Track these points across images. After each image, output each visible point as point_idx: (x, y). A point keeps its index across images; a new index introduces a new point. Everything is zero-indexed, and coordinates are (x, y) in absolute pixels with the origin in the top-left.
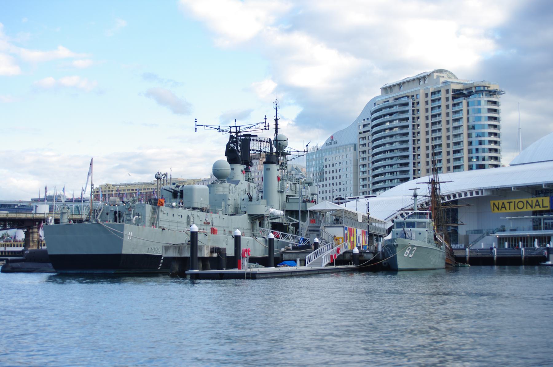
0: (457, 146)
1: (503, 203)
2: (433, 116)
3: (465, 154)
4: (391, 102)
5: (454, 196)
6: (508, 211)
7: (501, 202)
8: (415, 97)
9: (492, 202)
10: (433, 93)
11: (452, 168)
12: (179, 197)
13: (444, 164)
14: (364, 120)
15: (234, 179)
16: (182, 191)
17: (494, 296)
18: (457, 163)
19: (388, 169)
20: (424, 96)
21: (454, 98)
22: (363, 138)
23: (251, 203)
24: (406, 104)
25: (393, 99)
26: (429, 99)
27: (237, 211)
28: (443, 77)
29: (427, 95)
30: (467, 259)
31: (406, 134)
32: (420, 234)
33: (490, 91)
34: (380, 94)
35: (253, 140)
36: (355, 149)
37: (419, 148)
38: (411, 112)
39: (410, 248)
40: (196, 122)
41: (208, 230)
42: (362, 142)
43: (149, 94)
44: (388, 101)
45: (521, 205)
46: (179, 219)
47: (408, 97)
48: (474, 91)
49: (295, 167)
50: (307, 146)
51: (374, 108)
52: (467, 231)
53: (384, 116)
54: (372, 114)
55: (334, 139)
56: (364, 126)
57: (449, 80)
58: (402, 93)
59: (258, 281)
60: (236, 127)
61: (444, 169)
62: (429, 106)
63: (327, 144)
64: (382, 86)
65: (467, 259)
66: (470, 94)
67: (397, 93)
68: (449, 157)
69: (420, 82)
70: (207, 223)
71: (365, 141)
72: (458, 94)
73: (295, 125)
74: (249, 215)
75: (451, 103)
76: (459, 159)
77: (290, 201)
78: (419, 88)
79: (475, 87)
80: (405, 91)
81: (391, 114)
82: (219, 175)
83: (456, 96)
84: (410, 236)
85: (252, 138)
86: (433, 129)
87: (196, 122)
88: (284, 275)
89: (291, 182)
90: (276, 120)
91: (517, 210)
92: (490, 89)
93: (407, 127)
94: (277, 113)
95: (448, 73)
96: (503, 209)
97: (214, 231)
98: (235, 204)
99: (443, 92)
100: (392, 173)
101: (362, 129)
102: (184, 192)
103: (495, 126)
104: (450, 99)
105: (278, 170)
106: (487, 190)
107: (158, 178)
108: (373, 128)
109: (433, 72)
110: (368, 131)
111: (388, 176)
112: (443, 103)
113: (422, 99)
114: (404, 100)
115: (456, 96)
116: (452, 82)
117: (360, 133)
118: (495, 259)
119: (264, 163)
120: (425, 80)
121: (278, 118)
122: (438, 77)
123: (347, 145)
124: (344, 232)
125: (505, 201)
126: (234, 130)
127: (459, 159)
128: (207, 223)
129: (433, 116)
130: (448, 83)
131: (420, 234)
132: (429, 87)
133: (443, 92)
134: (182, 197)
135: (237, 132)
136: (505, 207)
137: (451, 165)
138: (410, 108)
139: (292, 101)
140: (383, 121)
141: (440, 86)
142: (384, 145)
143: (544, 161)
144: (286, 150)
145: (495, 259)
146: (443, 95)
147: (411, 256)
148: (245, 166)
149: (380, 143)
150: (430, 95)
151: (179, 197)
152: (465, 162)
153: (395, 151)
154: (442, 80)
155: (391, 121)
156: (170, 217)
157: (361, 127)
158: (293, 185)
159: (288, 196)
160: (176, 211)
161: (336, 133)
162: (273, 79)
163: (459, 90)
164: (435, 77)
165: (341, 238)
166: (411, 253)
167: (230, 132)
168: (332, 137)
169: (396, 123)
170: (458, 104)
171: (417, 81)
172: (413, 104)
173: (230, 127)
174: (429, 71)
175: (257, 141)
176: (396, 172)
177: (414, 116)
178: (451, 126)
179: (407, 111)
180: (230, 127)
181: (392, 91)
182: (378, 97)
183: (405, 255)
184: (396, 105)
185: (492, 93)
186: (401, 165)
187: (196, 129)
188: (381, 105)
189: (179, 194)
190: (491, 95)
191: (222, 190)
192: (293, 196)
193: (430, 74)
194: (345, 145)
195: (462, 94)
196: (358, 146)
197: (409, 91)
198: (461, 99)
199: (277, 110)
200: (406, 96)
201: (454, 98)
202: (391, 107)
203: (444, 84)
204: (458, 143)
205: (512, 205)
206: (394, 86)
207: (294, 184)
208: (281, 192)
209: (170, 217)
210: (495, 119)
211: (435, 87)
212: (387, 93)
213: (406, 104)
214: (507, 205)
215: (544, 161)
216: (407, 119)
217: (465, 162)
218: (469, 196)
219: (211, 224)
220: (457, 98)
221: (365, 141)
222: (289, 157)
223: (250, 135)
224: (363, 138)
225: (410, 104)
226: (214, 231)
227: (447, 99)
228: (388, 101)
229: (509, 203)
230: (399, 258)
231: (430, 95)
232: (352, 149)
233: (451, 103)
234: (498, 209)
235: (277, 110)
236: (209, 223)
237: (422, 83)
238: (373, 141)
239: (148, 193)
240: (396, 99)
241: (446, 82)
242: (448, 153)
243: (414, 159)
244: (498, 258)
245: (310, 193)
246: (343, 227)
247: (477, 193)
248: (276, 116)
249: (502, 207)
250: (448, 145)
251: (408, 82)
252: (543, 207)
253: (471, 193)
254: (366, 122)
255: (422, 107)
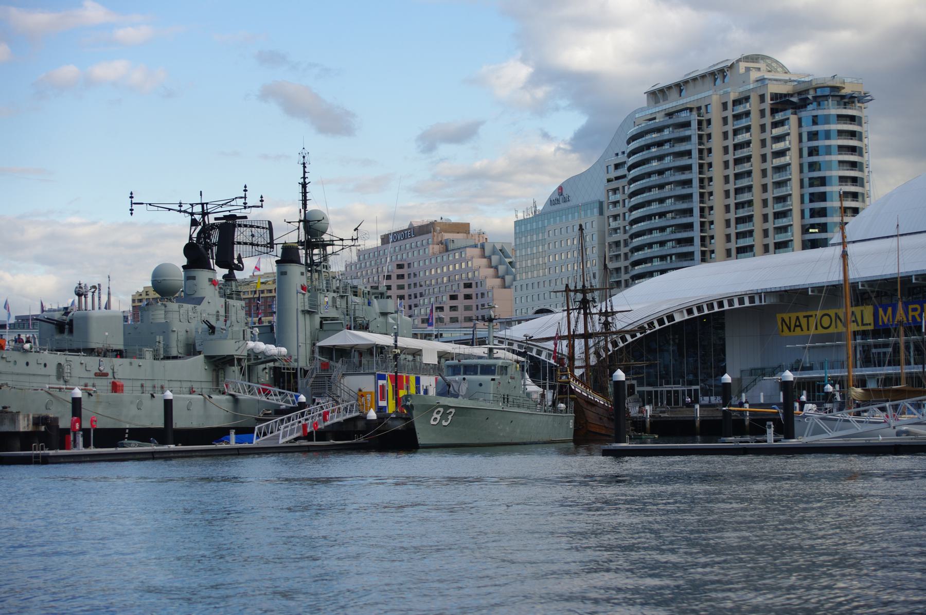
0: (780, 205)
1: (798, 318)
2: (737, 147)
3: (795, 221)
4: (660, 120)
5: (700, 309)
6: (805, 332)
7: (793, 316)
8: (703, 110)
9: (779, 316)
10: (736, 102)
11: (772, 247)
12: (66, 331)
13: (757, 240)
14: (617, 154)
15: (197, 295)
16: (71, 321)
17: (328, 481)
18: (781, 238)
19: (656, 250)
20: (721, 107)
21: (774, 111)
22: (615, 191)
23: (212, 337)
24: (687, 125)
25: (663, 113)
26: (729, 113)
27: (191, 350)
28: (759, 69)
29: (725, 106)
30: (648, 425)
31: (688, 183)
32: (481, 385)
33: (843, 97)
34: (645, 105)
35: (240, 226)
36: (601, 213)
37: (711, 208)
38: (695, 139)
39: (441, 410)
40: (131, 197)
41: (104, 385)
42: (613, 198)
43: (268, 93)
44: (655, 119)
45: (826, 321)
46: (43, 371)
47: (691, 109)
48: (810, 97)
49: (498, 247)
50: (356, 229)
51: (633, 130)
52: (742, 371)
53: (648, 147)
54: (628, 143)
55: (564, 193)
56: (617, 166)
57: (768, 76)
58: (684, 101)
59: (50, 466)
60: (202, 204)
61: (758, 248)
62: (730, 128)
63: (553, 202)
64: (648, 88)
65: (648, 425)
66: (803, 104)
67: (674, 102)
68: (766, 226)
69: (715, 80)
70: (101, 375)
71: (619, 197)
72: (781, 103)
73: (574, 150)
74: (206, 357)
75: (768, 120)
76: (784, 229)
77: (325, 327)
78: (710, 92)
79: (815, 89)
80: (689, 98)
81: (660, 144)
82: (162, 288)
83: (780, 107)
84: (456, 389)
85: (238, 221)
86: (737, 171)
87: (131, 197)
88: (138, 456)
89: (335, 295)
90: (304, 185)
91: (821, 331)
92: (843, 92)
93: (688, 168)
94: (305, 172)
95: (769, 61)
96: (798, 329)
97: (116, 387)
98: (187, 338)
99: (754, 99)
100: (663, 258)
101: (613, 174)
102: (74, 323)
103: (853, 165)
104: (768, 112)
105: (302, 274)
106: (769, 293)
107: (79, 295)
108: (630, 169)
109: (738, 61)
110: (624, 177)
111: (657, 264)
112: (754, 121)
113: (715, 114)
114: (684, 117)
115: (780, 107)
116: (770, 80)
117: (609, 181)
118: (747, 423)
119: (277, 262)
120: (724, 77)
121: (307, 181)
122: (748, 69)
123: (587, 204)
124: (376, 383)
125: (801, 315)
126: (198, 209)
127: (784, 229)
128: (101, 375)
129: (737, 147)
130: (767, 82)
131: (481, 385)
132: (729, 89)
133: (754, 99)
134: (71, 331)
135: (204, 214)
136: (800, 326)
137: (771, 241)
138: (693, 131)
139: (563, 103)
140: (646, 157)
141: (751, 86)
142: (648, 203)
143: (888, 237)
144: (326, 237)
145: (747, 423)
146: (753, 106)
147: (444, 423)
148: (226, 271)
149: (641, 201)
150: (730, 105)
151: (66, 331)
152: (796, 235)
153: (669, 216)
154: (754, 75)
155: (660, 158)
156: (21, 367)
157: (612, 168)
158: (338, 300)
159: (324, 319)
160: (32, 357)
161: (568, 181)
162: (524, 60)
163: (785, 95)
164: (742, 70)
165: (370, 393)
166: (444, 416)
167: (192, 214)
168: (560, 188)
169: (668, 162)
170: (781, 123)
171: (709, 80)
172: (700, 123)
173: (192, 205)
174: (734, 57)
175: (246, 226)
176: (671, 255)
177: (702, 147)
178: (768, 166)
179: (687, 139)
180: (192, 205)
181: (665, 99)
182: (642, 110)
183: (432, 422)
184: (668, 126)
185: (849, 100)
186: (680, 242)
187: (132, 210)
188: (644, 126)
189: (67, 326)
190: (845, 104)
191: (163, 316)
192: (333, 319)
193: (733, 64)
194: (583, 205)
195: (795, 101)
196: (605, 205)
197: (692, 98)
198: (788, 113)
199: (305, 167)
200: (686, 109)
201: (774, 111)
202: (660, 130)
203: (759, 84)
204: (782, 199)
205: (813, 322)
206: (669, 88)
207: (342, 297)
208: (309, 313)
209: (21, 367)
210: (853, 150)
211: (741, 89)
212: (657, 102)
213: (687, 125)
214: (804, 322)
215: (888, 237)
216: (688, 153)
217: (718, 244)
218: (736, 305)
219: (110, 376)
220: (782, 111)
221: (619, 197)
222: (329, 249)
223: (234, 217)
224: (615, 191)
225: (694, 125)
226: (116, 387)
227: (762, 113)
228: (655, 119)
229: (808, 317)
230: (418, 427)
231: (730, 105)
232: (596, 211)
233: (768, 120)
234: (789, 329)
235: (305, 167)
236: (106, 375)
237: (719, 81)
238: (633, 194)
239: (269, 300)
240: (670, 115)
241: (762, 80)
242: (765, 218)
243: (702, 231)
244: (702, 422)
245: (378, 311)
246: (374, 374)
247: (752, 300)
248: (304, 178)
249: (796, 326)
250: (765, 203)
251: (695, 79)
252: (863, 324)
253: (741, 301)
254: (621, 158)
255: (716, 129)
